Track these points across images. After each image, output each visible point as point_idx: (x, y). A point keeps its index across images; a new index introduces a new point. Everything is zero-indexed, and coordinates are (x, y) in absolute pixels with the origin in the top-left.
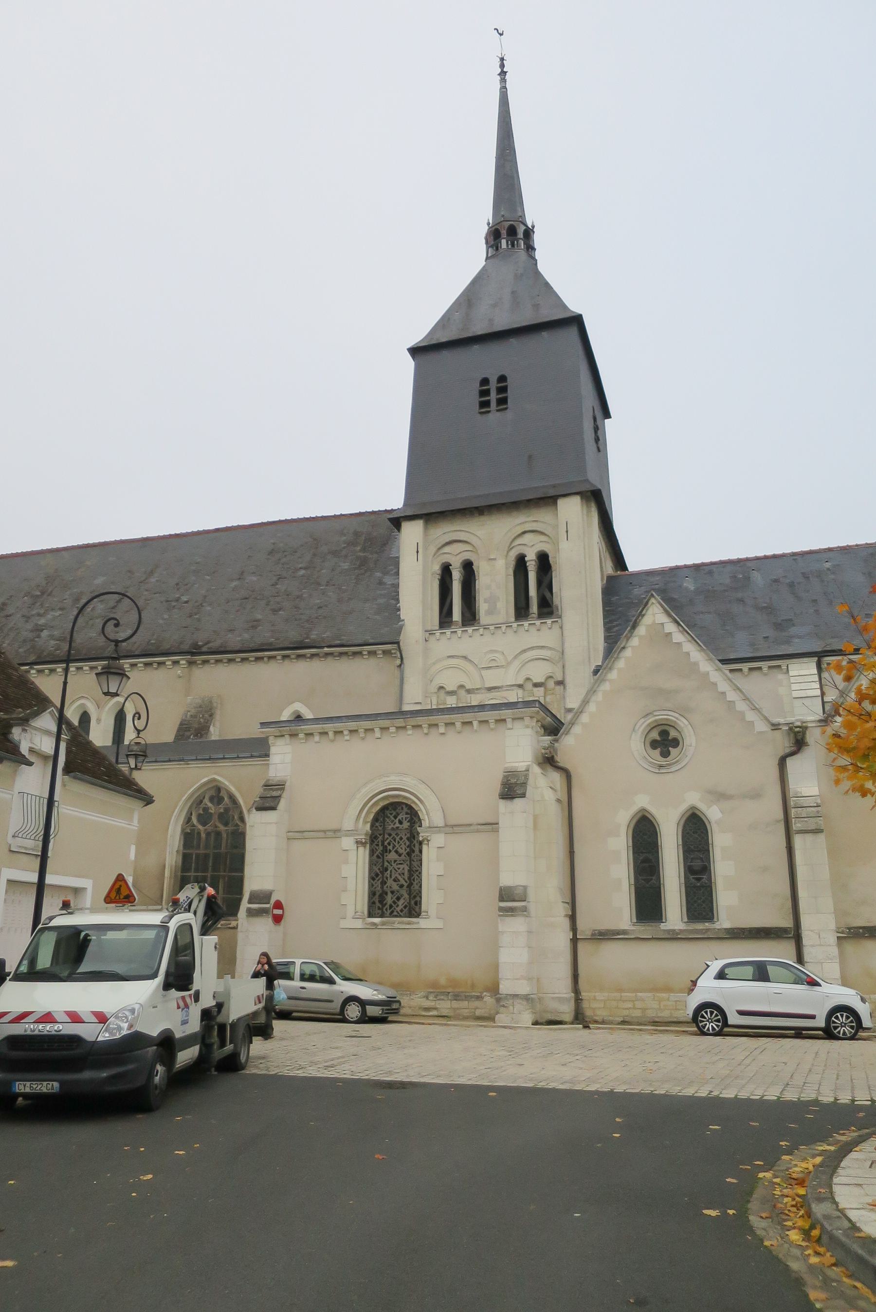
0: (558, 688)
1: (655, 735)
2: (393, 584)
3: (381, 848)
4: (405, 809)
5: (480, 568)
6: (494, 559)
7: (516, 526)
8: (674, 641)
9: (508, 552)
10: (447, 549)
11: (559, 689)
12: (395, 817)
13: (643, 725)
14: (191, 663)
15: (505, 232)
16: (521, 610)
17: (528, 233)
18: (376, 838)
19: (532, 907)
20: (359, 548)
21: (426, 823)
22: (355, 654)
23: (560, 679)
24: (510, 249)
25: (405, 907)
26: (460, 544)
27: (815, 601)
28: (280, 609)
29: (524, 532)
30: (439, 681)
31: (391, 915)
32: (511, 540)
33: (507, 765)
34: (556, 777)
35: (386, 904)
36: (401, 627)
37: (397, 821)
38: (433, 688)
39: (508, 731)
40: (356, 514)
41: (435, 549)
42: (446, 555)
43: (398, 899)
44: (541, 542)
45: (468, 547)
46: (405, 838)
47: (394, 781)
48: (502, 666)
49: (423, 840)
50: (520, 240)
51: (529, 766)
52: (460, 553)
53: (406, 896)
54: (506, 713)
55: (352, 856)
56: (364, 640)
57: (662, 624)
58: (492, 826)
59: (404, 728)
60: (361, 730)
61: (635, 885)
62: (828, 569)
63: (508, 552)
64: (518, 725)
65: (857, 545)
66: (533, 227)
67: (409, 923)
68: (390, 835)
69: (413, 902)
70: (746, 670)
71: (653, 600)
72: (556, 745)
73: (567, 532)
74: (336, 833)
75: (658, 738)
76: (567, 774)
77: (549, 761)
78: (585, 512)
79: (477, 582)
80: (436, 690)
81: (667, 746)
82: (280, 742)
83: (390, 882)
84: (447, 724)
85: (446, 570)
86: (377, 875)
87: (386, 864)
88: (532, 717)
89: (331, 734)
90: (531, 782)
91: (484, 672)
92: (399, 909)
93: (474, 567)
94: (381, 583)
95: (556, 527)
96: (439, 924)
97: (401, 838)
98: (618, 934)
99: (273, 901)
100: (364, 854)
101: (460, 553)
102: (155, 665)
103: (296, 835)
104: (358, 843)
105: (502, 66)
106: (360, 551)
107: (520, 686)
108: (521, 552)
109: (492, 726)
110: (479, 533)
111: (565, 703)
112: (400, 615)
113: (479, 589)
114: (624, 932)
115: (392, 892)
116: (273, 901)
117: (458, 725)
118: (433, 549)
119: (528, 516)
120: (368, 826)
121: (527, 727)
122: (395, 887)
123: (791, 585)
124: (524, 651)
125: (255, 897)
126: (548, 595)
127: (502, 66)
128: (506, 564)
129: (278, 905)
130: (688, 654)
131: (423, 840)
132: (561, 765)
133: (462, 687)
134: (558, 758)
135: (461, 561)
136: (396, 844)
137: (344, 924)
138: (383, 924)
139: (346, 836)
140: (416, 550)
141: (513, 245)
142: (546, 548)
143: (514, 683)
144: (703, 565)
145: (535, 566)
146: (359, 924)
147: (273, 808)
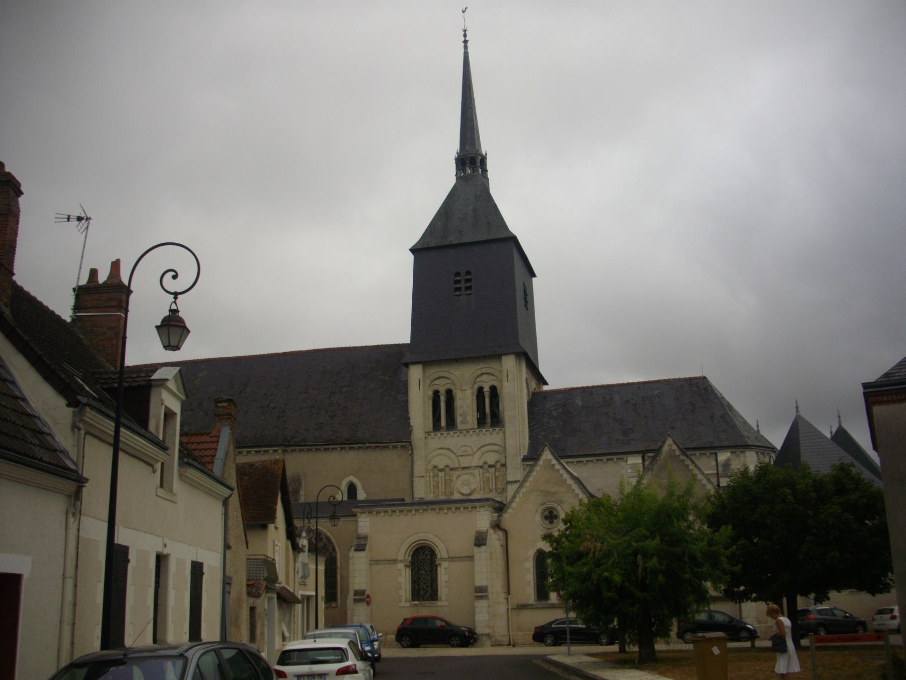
0: (502, 468)
1: (546, 513)
3: (417, 568)
4: (428, 549)
6: (465, 390)
8: (556, 468)
9: (473, 385)
10: (437, 382)
11: (503, 469)
12: (423, 553)
13: (541, 509)
14: (284, 451)
15: (468, 161)
16: (481, 422)
18: (414, 563)
19: (490, 595)
21: (439, 556)
22: (384, 447)
23: (503, 463)
25: (430, 596)
26: (445, 379)
27: (646, 417)
28: (335, 415)
29: (482, 374)
30: (433, 463)
31: (423, 600)
33: (477, 529)
34: (500, 533)
35: (420, 595)
36: (411, 431)
37: (424, 555)
38: (430, 467)
39: (477, 513)
42: (437, 386)
43: (426, 592)
45: (450, 382)
46: (428, 563)
47: (422, 536)
48: (471, 455)
49: (438, 565)
51: (487, 530)
53: (430, 591)
54: (477, 504)
55: (403, 572)
57: (551, 460)
58: (471, 558)
59: (427, 510)
60: (405, 511)
61: (537, 584)
62: (656, 395)
63: (473, 385)
64: (482, 509)
65: (674, 379)
66: (486, 154)
67: (433, 604)
68: (421, 562)
69: (433, 594)
70: (605, 460)
71: (546, 448)
72: (501, 518)
73: (507, 376)
74: (395, 561)
75: (548, 515)
76: (506, 533)
77: (497, 526)
78: (518, 363)
79: (455, 403)
80: (432, 468)
81: (552, 519)
82: (363, 516)
83: (422, 585)
84: (448, 509)
85: (436, 394)
86: (415, 581)
87: (420, 576)
88: (489, 506)
89: (390, 512)
90: (488, 537)
91: (460, 458)
92: (427, 597)
93: (453, 394)
95: (501, 371)
96: (447, 604)
97: (427, 564)
98: (529, 606)
99: (366, 595)
100: (409, 571)
102: (262, 453)
103: (374, 562)
104: (406, 566)
105: (465, 36)
107: (481, 467)
108: (481, 385)
109: (470, 510)
110: (455, 373)
111: (506, 478)
112: (410, 422)
114: (532, 605)
115: (423, 589)
116: (366, 595)
117: (453, 509)
118: (428, 382)
120: (410, 558)
121: (487, 510)
122: (425, 587)
123: (635, 405)
124: (483, 446)
125: (357, 593)
126: (496, 411)
127: (465, 36)
128: (472, 393)
129: (368, 596)
130: (562, 475)
131: (438, 565)
132: (503, 527)
133: (447, 466)
134: (501, 525)
136: (424, 566)
137: (401, 605)
138: (419, 604)
139: (400, 563)
140: (418, 383)
142: (496, 384)
143: (477, 465)
144: (588, 387)
146: (408, 604)
147: (364, 550)
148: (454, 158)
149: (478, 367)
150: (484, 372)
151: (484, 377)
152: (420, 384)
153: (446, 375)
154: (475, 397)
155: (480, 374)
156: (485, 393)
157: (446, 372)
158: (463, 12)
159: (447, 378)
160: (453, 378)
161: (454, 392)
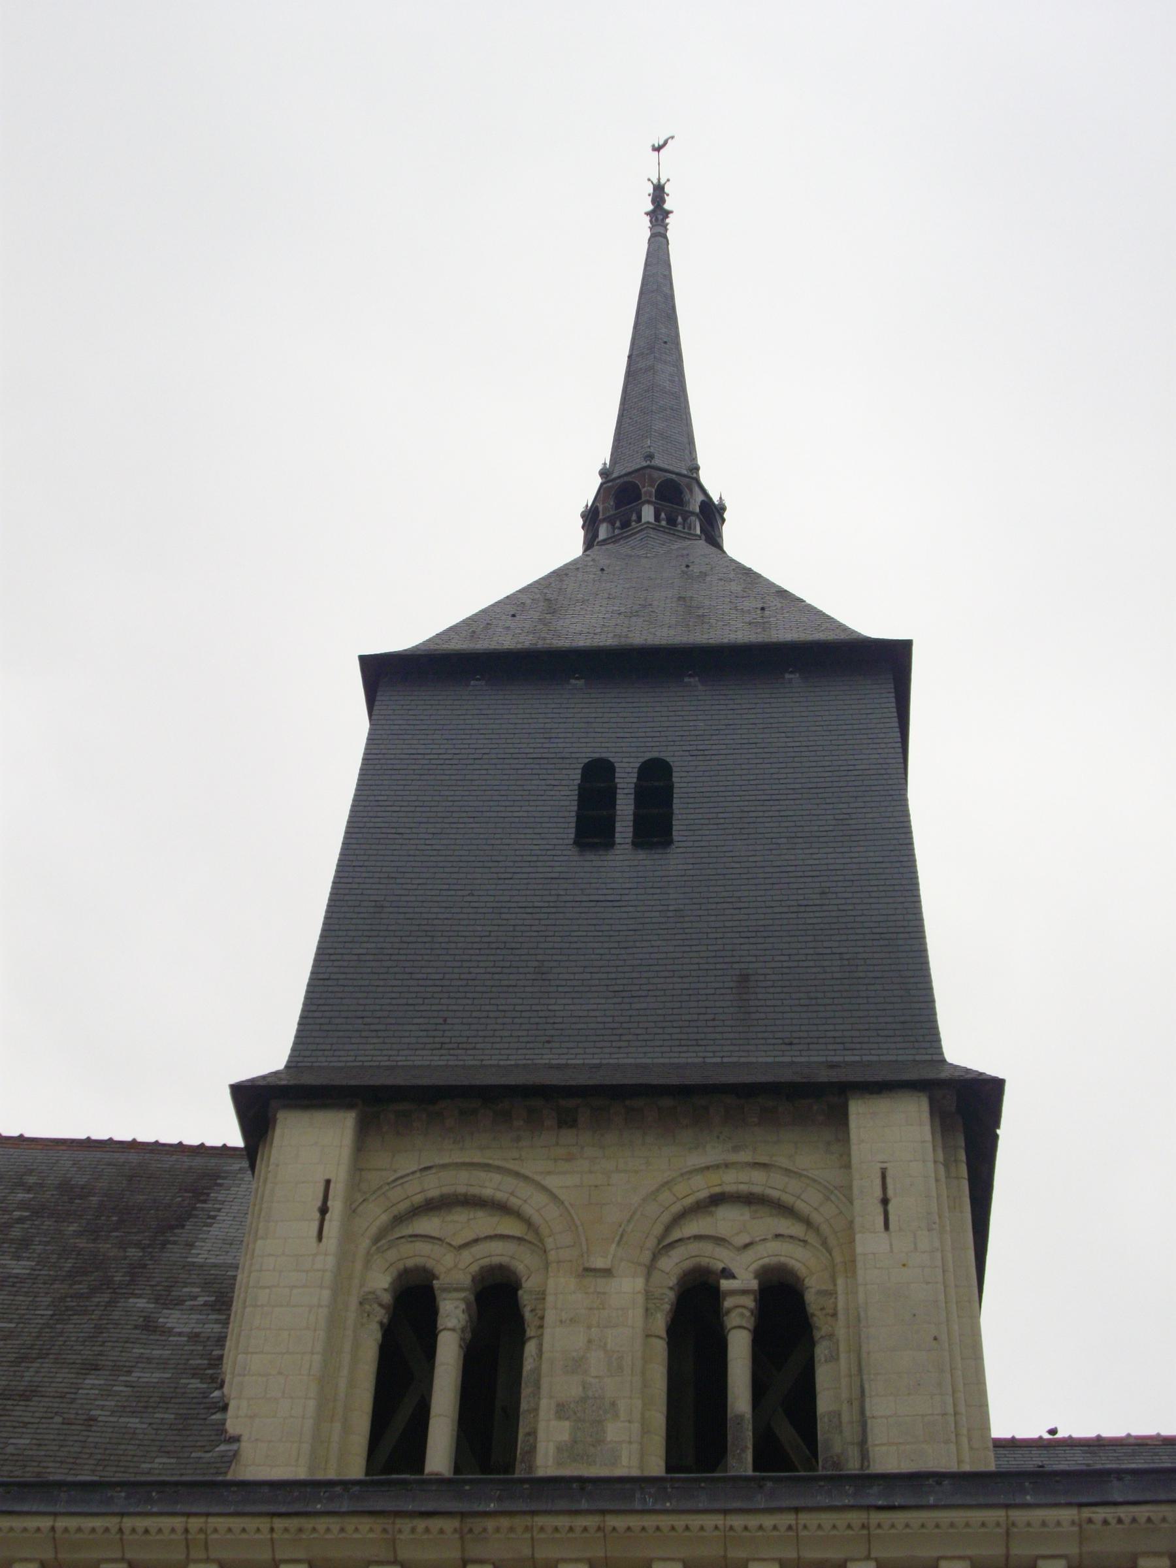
2: (197, 1335)
5: (550, 1299)
6: (607, 1272)
7: (690, 1172)
10: (428, 1225)
17: (712, 514)
20: (73, 1228)
24: (663, 527)
29: (717, 1200)
32: (666, 1218)
40: (73, 1141)
41: (384, 1218)
44: (778, 1236)
45: (510, 1227)
50: (693, 518)
52: (476, 1241)
56: (470, 688)
63: (655, 1257)
73: (885, 1201)
79: (530, 1348)
94: (149, 1326)
101: (476, 1241)
106: (79, 1234)
110: (551, 1182)
113: (537, 1370)
118: (376, 1215)
119: (736, 1149)
126: (786, 1433)
128: (648, 1295)
135: (475, 1268)
141: (672, 521)
145: (752, 1312)
148: (600, 467)
149: (696, 1160)
150: (729, 1188)
151: (727, 1220)
152: (324, 1210)
153: (490, 1186)
154: (660, 1324)
155: (703, 1194)
156: (728, 1303)
157: (499, 1169)
158: (657, 149)
159: (501, 1208)
160: (532, 1203)
161: (529, 1284)
